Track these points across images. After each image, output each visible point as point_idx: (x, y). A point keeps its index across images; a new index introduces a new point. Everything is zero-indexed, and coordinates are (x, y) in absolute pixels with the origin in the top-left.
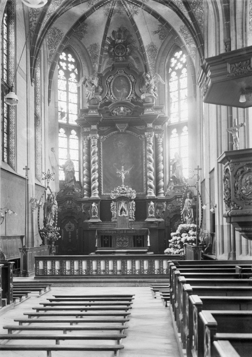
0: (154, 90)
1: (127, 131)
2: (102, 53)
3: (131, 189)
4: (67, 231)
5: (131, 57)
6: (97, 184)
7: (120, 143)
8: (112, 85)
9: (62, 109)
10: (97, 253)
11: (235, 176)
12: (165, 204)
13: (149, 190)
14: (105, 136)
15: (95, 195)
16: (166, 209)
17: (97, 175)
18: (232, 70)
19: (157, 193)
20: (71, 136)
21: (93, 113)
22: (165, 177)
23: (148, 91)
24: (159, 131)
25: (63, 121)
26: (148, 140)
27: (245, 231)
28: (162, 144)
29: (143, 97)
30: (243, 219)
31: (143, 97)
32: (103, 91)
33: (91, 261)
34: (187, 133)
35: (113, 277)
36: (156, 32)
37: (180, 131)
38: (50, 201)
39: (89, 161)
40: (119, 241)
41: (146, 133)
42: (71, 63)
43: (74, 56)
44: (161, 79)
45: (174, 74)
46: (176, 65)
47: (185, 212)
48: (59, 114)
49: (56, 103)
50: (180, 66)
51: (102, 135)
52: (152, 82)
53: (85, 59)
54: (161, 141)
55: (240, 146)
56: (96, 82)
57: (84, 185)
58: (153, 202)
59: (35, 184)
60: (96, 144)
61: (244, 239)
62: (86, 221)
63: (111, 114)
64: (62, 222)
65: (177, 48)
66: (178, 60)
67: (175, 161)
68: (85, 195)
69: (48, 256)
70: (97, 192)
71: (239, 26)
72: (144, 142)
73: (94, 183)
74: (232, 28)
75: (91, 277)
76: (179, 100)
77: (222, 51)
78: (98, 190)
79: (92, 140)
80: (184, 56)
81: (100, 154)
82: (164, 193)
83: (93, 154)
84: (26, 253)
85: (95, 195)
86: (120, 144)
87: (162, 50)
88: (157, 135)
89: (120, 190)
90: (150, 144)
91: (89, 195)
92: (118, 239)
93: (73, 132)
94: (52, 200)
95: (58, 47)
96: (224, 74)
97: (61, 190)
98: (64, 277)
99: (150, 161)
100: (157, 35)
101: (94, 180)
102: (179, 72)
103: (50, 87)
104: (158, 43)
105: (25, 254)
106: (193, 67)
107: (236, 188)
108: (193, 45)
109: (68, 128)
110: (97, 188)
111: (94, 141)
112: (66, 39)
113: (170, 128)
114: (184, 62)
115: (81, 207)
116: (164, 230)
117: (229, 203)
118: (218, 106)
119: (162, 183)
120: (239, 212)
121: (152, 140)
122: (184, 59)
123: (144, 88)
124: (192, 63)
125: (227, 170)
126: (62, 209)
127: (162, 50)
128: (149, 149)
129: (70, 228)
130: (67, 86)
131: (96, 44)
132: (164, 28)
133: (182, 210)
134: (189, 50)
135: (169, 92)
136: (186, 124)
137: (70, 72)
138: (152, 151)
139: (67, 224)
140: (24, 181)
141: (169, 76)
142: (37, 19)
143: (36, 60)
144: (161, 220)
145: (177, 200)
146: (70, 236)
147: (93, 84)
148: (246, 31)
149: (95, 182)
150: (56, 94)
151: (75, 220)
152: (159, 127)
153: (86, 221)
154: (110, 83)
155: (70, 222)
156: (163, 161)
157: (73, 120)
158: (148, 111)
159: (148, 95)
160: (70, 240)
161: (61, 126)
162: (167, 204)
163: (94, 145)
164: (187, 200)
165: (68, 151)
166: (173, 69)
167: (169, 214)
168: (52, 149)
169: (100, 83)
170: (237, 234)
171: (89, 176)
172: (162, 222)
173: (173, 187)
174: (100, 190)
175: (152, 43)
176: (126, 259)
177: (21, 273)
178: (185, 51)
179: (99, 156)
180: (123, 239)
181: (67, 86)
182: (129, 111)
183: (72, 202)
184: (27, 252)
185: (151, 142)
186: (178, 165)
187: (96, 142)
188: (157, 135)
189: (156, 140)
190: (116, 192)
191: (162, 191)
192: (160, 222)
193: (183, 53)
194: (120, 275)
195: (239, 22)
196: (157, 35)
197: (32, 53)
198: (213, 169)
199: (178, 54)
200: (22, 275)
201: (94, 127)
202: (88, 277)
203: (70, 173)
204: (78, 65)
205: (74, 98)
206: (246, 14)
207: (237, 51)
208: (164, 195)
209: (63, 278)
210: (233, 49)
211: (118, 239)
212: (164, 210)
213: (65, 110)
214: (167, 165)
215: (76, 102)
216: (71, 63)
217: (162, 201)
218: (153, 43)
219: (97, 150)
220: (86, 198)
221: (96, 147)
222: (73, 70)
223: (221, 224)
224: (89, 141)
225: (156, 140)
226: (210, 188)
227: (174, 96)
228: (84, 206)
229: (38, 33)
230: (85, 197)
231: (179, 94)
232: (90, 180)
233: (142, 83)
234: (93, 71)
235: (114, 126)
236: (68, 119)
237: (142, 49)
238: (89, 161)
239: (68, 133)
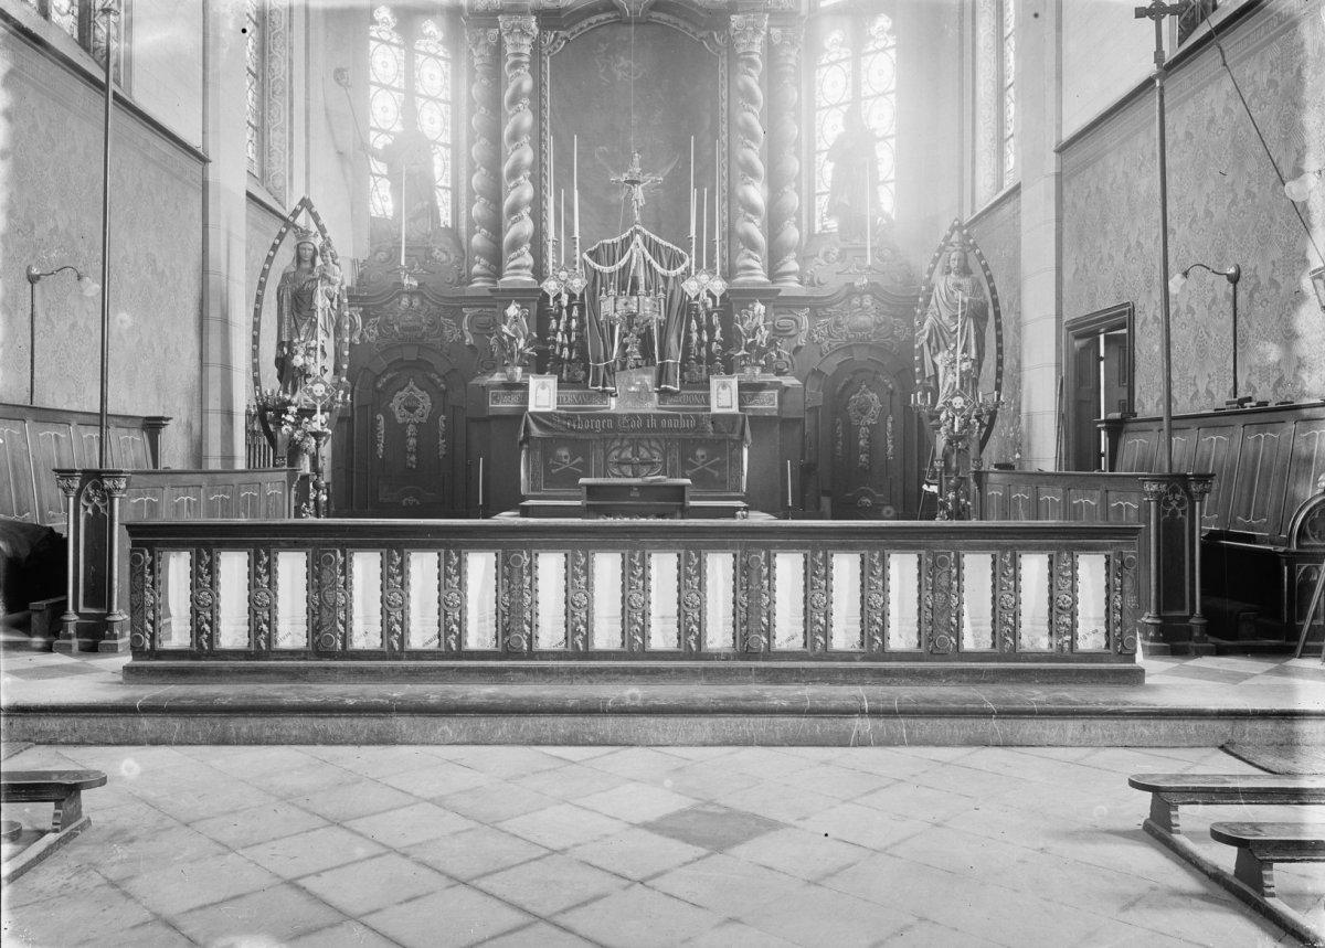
1: (655, 14)
4: (400, 420)
6: (527, 227)
7: (623, 62)
10: (526, 512)
12: (805, 319)
13: (742, 255)
14: (562, 33)
15: (518, 273)
16: (810, 338)
20: (420, 45)
26: (740, 50)
33: (525, 559)
35: (680, 671)
38: (308, 266)
40: (620, 464)
51: (552, 28)
54: (792, 61)
57: (471, 233)
58: (763, 302)
59: (249, 195)
60: (525, 59)
64: (380, 386)
68: (477, 275)
69: (287, 521)
70: (529, 260)
73: (514, 223)
75: (527, 671)
78: (532, 252)
79: (508, 41)
81: (542, 107)
84: (103, 499)
85: (518, 273)
86: (622, 68)
88: (775, 32)
92: (616, 453)
94: (319, 262)
97: (379, 251)
98: (335, 669)
105: (96, 509)
110: (528, 246)
111: (516, 45)
115: (459, 325)
116: (799, 420)
126: (379, 330)
128: (747, 87)
129: (411, 410)
133: (922, 324)
138: (759, 129)
139: (399, 394)
140: (198, 167)
145: (856, 301)
146: (412, 441)
149: (521, 218)
151: (433, 375)
155: (411, 384)
160: (413, 458)
162: (814, 315)
163: (516, 65)
167: (819, 359)
173: (837, 250)
176: (767, 547)
177: (71, 631)
179: (538, 112)
180: (636, 453)
183: (422, 303)
184: (107, 496)
185: (756, 58)
187: (527, 51)
188: (775, 32)
189: (771, 50)
194: (727, 658)
200: (75, 642)
202: (504, 670)
203: (415, 187)
208: (801, 283)
209: (327, 674)
211: (616, 453)
212: (802, 341)
219: (527, 84)
220: (477, 288)
221: (524, 71)
224: (497, 50)
225: (771, 50)
228: (470, 322)
230: (478, 284)
232: (498, 212)
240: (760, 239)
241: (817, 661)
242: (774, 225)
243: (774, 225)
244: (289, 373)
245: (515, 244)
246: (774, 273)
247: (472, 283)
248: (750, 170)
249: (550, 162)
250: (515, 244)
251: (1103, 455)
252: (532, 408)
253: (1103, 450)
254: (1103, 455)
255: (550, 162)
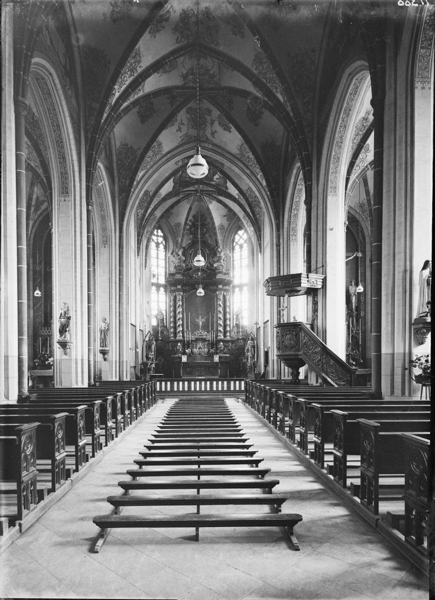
0: (224, 261)
2: (184, 230)
3: (206, 333)
5: (206, 235)
6: (181, 329)
8: (192, 256)
9: (153, 271)
11: (282, 336)
15: (180, 337)
17: (181, 323)
18: (281, 284)
19: (225, 336)
20: (160, 292)
21: (179, 276)
22: (231, 323)
23: (219, 261)
24: (227, 290)
25: (154, 281)
27: (287, 363)
28: (229, 300)
29: (215, 265)
30: (286, 357)
31: (215, 265)
32: (185, 260)
34: (247, 292)
36: (224, 216)
37: (241, 290)
39: (175, 311)
41: (217, 292)
42: (161, 236)
43: (162, 232)
44: (228, 252)
45: (237, 248)
46: (239, 240)
47: (248, 350)
48: (152, 275)
49: (150, 268)
50: (242, 242)
52: (222, 254)
53: (171, 234)
55: (285, 320)
56: (180, 253)
61: (286, 367)
62: (173, 356)
63: (191, 277)
65: (240, 228)
66: (241, 237)
67: (238, 313)
70: (181, 335)
71: (285, 236)
72: (215, 299)
74: (281, 237)
76: (241, 267)
77: (275, 275)
80: (245, 234)
82: (230, 336)
83: (179, 307)
85: (180, 337)
87: (229, 229)
88: (225, 293)
89: (198, 334)
90: (220, 300)
91: (175, 336)
93: (162, 289)
95: (152, 227)
96: (277, 286)
99: (221, 312)
100: (225, 218)
101: (179, 326)
102: (241, 247)
103: (146, 256)
104: (226, 223)
106: (252, 244)
107: (283, 342)
108: (252, 229)
109: (158, 286)
112: (159, 221)
113: (234, 287)
114: (245, 239)
117: (279, 349)
118: (275, 298)
119: (228, 329)
120: (284, 353)
121: (221, 297)
122: (245, 237)
123: (216, 259)
124: (252, 241)
125: (278, 332)
127: (229, 229)
130: (158, 254)
131: (179, 223)
132: (231, 215)
134: (249, 231)
135: (233, 261)
136: (246, 285)
137: (160, 244)
138: (222, 305)
141: (233, 249)
142: (143, 211)
143: (141, 240)
144: (228, 355)
147: (179, 255)
148: (289, 240)
150: (150, 260)
152: (227, 287)
153: (173, 356)
154: (191, 254)
156: (229, 312)
157: (162, 281)
158: (219, 276)
159: (219, 264)
161: (153, 284)
162: (232, 344)
163: (179, 300)
164: (249, 342)
165: (158, 303)
166: (237, 243)
168: (148, 302)
169: (184, 254)
170: (282, 364)
171: (175, 322)
172: (228, 357)
174: (183, 333)
175: (222, 223)
178: (246, 231)
181: (158, 254)
182: (205, 275)
185: (221, 299)
186: (240, 316)
188: (225, 293)
189: (224, 296)
190: (195, 335)
191: (228, 334)
192: (227, 357)
193: (244, 232)
195: (285, 233)
196: (225, 218)
197: (138, 236)
198: (268, 320)
199: (241, 232)
201: (179, 287)
204: (165, 238)
205: (162, 263)
206: (290, 230)
207: (284, 276)
210: (282, 274)
212: (230, 348)
213: (155, 273)
214: (232, 315)
215: (164, 266)
216: (161, 236)
217: (228, 341)
218: (222, 223)
219: (181, 304)
221: (180, 301)
222: (162, 243)
223: (272, 359)
225: (224, 296)
226: (264, 334)
227: (237, 263)
229: (143, 220)
230: (172, 338)
231: (241, 262)
233: (215, 254)
234: (177, 243)
235: (194, 286)
236: (158, 279)
237: (214, 228)
238: (175, 311)
239: (158, 290)
240: (222, 330)
241: (235, 391)
242: (225, 326)
243: (225, 326)
244: (148, 358)
245: (179, 332)
246: (225, 336)
247: (166, 326)
248: (220, 306)
249: (185, 317)
250: (179, 332)
251: (199, 457)
252: (183, 361)
253: (201, 457)
254: (199, 457)
255: (185, 317)
